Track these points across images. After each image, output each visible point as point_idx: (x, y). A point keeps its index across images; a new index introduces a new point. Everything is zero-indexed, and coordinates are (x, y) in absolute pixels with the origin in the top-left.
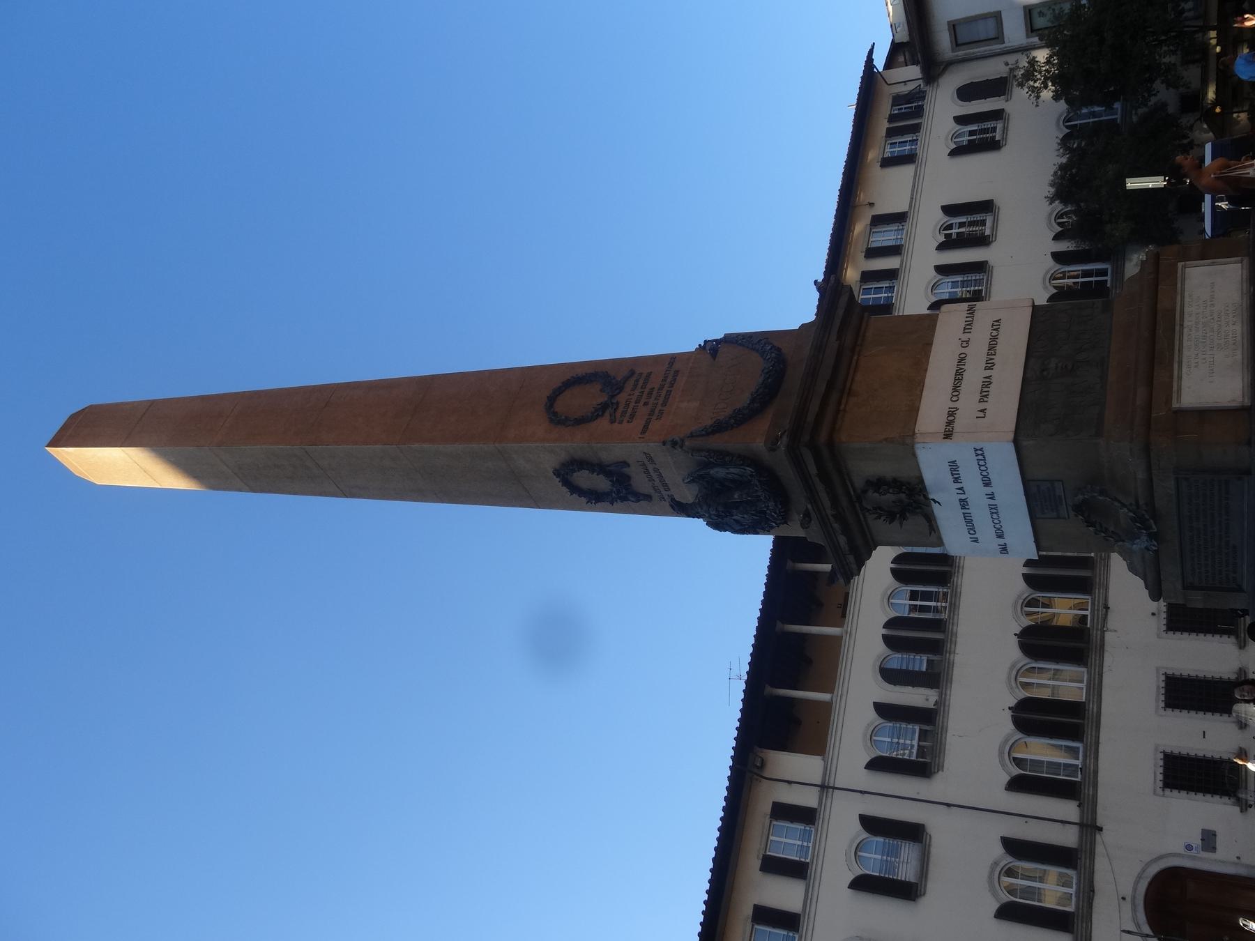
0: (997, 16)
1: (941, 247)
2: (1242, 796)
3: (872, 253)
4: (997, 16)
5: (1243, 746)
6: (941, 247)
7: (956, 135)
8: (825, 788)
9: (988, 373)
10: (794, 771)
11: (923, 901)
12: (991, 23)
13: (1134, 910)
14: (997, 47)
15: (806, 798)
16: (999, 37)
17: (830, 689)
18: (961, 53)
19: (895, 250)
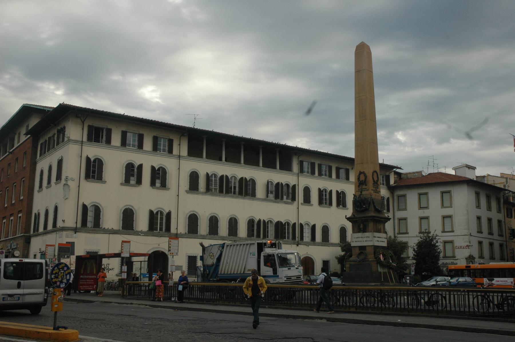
0: (405, 209)
1: (337, 192)
2: (393, 237)
3: (320, 166)
4: (405, 209)
5: (489, 217)
6: (337, 192)
7: (215, 176)
8: (179, 157)
9: (447, 212)
10: (182, 148)
11: (151, 188)
12: (404, 207)
13: (156, 248)
14: (396, 209)
15: (175, 151)
16: (399, 209)
17: (207, 157)
18: (396, 198)
19: (338, 177)
